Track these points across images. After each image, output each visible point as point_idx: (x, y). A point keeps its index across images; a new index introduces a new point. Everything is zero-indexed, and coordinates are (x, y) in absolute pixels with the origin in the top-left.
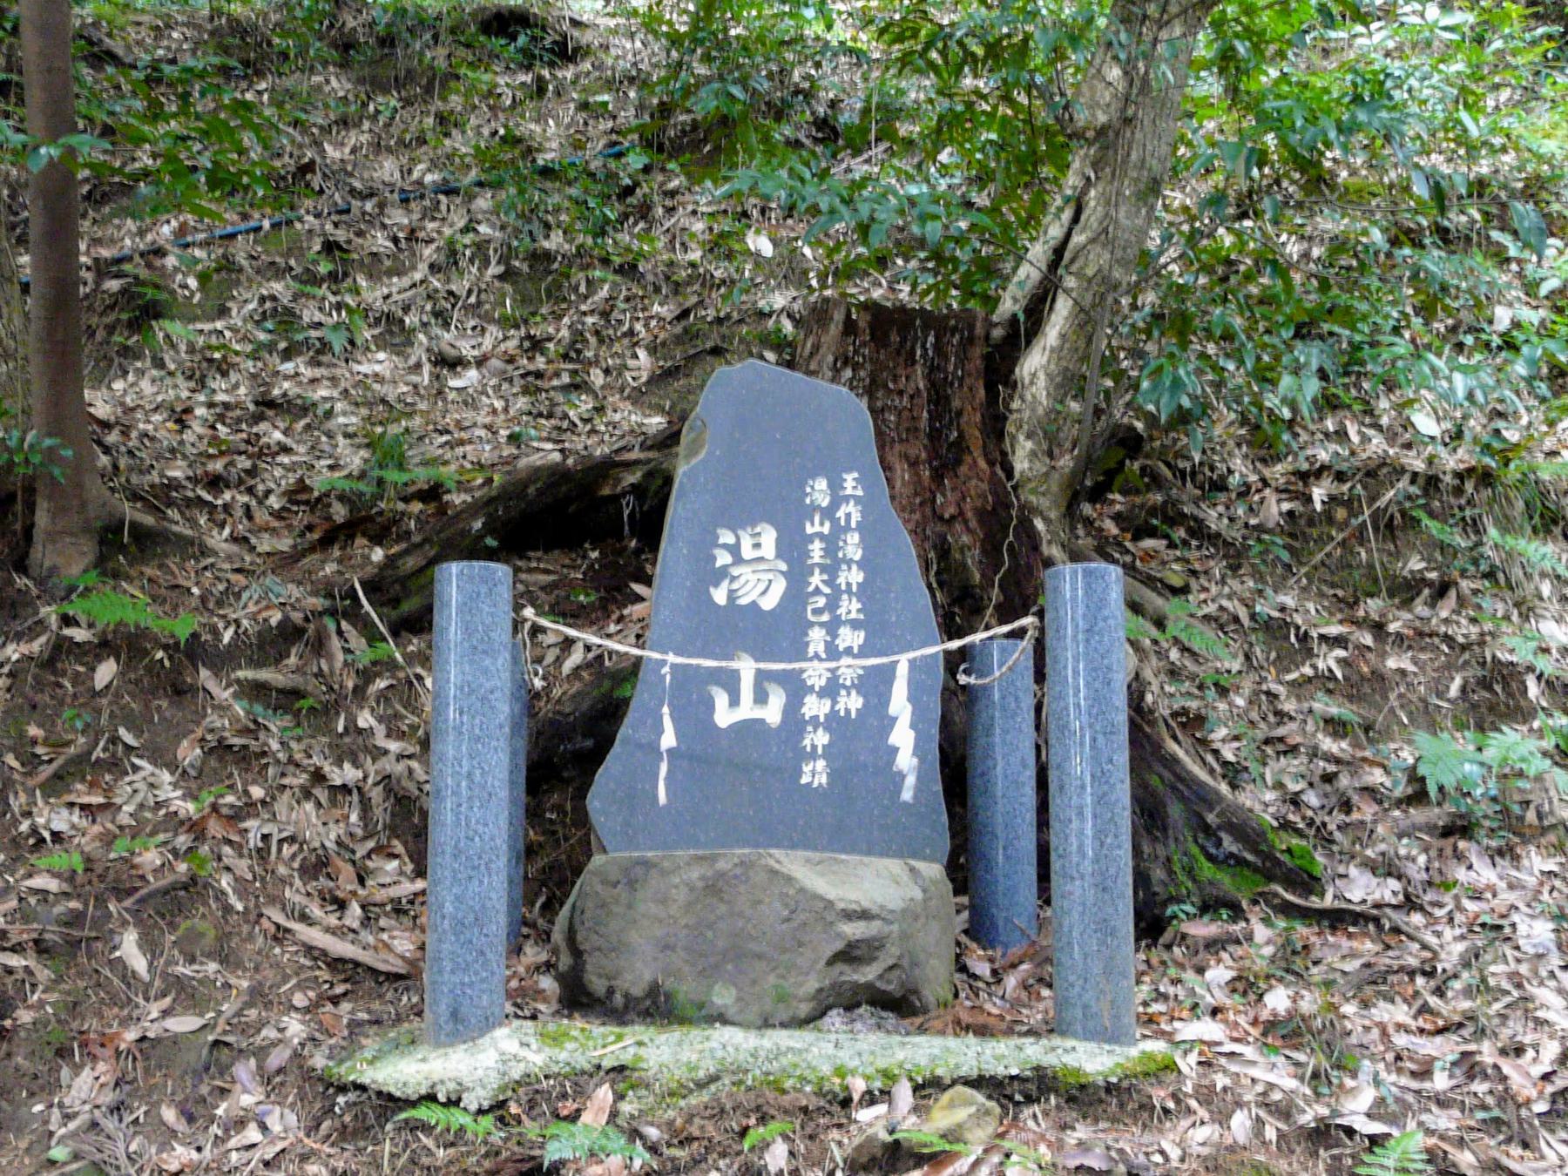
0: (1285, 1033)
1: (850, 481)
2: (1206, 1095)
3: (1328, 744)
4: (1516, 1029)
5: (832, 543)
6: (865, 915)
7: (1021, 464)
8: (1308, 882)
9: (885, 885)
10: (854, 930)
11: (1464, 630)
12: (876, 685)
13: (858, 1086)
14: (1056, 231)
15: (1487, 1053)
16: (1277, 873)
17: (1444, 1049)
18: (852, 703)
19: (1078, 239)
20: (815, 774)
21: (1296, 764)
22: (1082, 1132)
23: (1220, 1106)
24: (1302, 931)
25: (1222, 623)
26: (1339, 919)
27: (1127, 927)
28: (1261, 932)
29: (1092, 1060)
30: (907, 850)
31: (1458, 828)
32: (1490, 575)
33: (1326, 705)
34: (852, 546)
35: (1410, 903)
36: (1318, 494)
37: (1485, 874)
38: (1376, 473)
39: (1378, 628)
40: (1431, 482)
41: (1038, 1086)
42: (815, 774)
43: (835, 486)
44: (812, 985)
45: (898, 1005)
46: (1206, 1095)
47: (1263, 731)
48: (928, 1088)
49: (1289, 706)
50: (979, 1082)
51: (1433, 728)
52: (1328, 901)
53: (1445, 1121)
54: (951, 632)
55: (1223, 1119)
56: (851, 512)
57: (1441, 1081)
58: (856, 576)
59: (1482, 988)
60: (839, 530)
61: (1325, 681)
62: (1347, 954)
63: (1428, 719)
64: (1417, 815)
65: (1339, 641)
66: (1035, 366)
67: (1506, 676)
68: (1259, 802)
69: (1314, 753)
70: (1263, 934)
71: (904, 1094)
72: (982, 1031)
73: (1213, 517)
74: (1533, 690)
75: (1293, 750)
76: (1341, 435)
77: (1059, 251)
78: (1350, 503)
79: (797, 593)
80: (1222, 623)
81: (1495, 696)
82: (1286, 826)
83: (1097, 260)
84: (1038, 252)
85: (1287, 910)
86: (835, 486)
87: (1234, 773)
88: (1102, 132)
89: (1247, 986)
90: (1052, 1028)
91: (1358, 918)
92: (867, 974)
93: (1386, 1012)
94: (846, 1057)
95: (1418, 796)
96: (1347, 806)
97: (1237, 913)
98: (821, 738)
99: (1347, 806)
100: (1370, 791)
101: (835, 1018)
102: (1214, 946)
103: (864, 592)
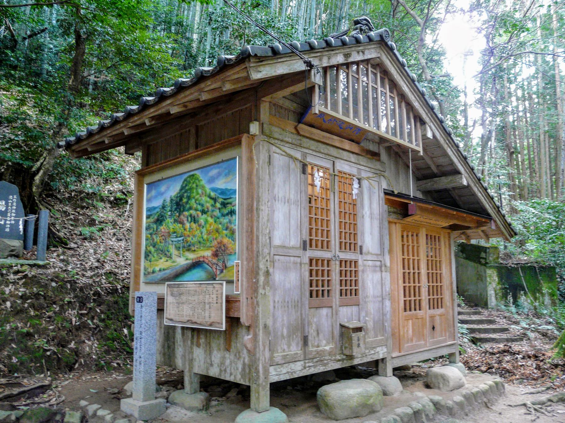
0: (62, 261)
1: (15, 197)
2: (53, 266)
3: (71, 228)
4: (88, 261)
5: (12, 203)
6: (14, 247)
7: (34, 190)
8: (66, 244)
9: (17, 244)
10: (13, 248)
11: (90, 214)
12: (17, 222)
13: (14, 265)
14: (42, 161)
15: (84, 263)
16: (63, 243)
17: (79, 263)
18: (13, 222)
19: (45, 163)
20: (7, 230)
21: (66, 230)
22: (39, 270)
23: (55, 268)
24: (66, 250)
25: (58, 211)
26: (70, 249)
27: (46, 249)
28: (60, 250)
29: (41, 263)
30: (19, 239)
31: (85, 239)
32: (94, 207)
33: (71, 222)
34: (15, 204)
35: (78, 247)
36: (73, 194)
37: (87, 244)
38: (81, 192)
39: (79, 213)
40: (88, 194)
41: (35, 265)
42: (7, 230)
43: (13, 197)
44: (7, 254)
45: (17, 256)
46: (53, 266)
47: (63, 225)
48: (22, 265)
49: (66, 222)
50: (28, 265)
51: (84, 226)
52: (68, 247)
53: (78, 270)
54: (26, 216)
55: (55, 269)
56: (15, 200)
57: (79, 266)
58: (15, 208)
59: (85, 257)
60: (13, 202)
61: (71, 219)
62: (70, 252)
63: (83, 225)
64: (81, 237)
65: (73, 214)
66: (37, 178)
67: (94, 220)
68: (61, 234)
69: (69, 229)
70: (60, 250)
71: (19, 266)
72: (27, 260)
73: (59, 196)
74: (97, 222)
75: (66, 228)
76: (77, 186)
77: (42, 164)
78: (77, 196)
79: (7, 209)
80: (58, 211)
81: (92, 223)
82: (65, 238)
83: (47, 166)
84: (39, 163)
85: (64, 247)
86: (13, 197)
87: (58, 231)
88: (49, 150)
89: (58, 256)
90: (36, 259)
91: (72, 249)
92: (14, 253)
93: (74, 259)
94: (12, 262)
95: (81, 235)
96: (72, 235)
97: (58, 248)
98: (9, 226)
99: (72, 235)
100: (75, 234)
101: (9, 258)
102: (55, 251)
103: (16, 210)
